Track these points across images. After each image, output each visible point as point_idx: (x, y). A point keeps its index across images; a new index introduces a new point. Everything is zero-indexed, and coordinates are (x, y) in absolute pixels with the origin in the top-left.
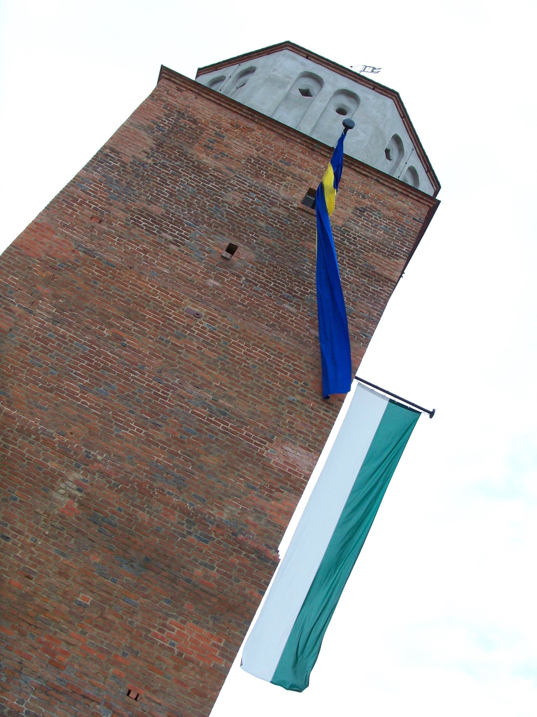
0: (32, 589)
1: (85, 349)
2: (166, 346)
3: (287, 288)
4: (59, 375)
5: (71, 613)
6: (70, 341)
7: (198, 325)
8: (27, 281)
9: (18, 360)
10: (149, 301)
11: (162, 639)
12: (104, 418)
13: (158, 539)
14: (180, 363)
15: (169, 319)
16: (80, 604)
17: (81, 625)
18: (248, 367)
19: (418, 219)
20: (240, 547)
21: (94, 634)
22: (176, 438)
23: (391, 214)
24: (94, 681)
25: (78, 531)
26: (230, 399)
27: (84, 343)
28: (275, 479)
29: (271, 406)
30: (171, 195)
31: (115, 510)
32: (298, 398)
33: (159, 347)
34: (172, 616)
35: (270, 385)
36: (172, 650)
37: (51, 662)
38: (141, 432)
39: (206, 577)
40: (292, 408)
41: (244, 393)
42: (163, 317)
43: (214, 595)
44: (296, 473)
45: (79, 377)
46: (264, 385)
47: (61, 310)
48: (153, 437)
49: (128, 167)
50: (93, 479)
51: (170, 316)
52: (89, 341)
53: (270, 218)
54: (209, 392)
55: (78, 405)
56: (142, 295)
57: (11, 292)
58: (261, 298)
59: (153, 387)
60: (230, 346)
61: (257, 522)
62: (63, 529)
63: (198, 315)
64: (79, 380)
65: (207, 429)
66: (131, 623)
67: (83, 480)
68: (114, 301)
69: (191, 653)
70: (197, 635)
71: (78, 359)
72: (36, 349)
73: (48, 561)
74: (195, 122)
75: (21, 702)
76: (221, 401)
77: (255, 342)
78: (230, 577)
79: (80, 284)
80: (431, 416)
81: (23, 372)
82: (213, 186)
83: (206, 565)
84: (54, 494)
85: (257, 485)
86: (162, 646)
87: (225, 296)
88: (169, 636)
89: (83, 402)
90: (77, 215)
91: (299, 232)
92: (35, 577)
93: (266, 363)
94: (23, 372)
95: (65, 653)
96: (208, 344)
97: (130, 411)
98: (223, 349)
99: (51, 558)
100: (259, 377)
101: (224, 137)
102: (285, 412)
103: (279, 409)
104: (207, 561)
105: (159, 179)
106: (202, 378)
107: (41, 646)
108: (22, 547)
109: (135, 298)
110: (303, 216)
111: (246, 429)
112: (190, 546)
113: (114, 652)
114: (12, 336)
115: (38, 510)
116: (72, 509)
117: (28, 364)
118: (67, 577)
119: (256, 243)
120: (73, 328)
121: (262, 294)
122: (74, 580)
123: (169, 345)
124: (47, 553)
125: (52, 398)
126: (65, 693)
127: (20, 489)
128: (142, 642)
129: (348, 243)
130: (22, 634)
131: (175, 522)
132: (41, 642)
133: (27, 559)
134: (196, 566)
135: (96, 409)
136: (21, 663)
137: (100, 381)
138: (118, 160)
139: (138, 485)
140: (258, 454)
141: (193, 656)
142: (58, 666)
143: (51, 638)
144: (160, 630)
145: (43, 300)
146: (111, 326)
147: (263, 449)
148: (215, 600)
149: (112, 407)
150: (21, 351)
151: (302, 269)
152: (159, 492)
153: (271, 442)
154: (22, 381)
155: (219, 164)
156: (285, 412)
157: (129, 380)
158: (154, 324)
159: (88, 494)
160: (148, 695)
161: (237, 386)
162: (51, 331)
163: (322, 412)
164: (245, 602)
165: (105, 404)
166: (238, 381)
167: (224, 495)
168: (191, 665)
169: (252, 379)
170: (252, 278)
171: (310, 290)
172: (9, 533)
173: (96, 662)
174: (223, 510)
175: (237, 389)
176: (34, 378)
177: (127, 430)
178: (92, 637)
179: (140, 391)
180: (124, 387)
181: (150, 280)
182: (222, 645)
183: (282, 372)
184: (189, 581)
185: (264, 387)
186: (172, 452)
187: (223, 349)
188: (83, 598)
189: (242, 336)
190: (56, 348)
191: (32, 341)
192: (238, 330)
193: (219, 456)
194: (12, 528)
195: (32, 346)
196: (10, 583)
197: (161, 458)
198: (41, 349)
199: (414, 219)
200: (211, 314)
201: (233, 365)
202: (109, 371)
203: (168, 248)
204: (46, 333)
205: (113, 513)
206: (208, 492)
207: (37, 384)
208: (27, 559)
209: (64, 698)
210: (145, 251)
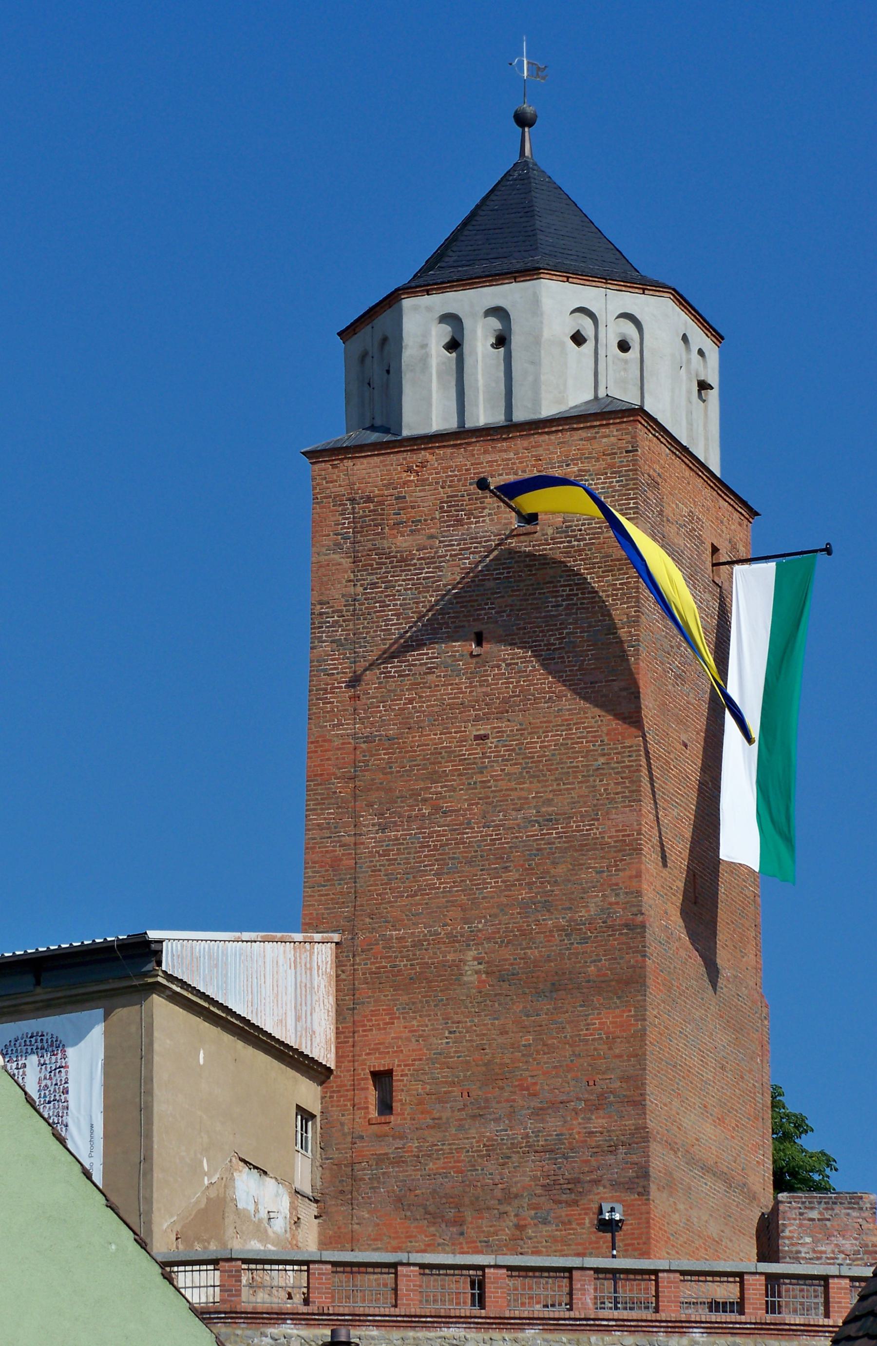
0: (490, 1055)
1: (419, 838)
2: (476, 788)
3: (545, 645)
4: (414, 877)
5: (523, 1055)
6: (404, 839)
7: (491, 748)
8: (340, 807)
9: (377, 885)
10: (441, 753)
11: (591, 1035)
12: (466, 890)
13: (552, 964)
14: (494, 797)
15: (465, 759)
16: (525, 1046)
17: (535, 1059)
18: (549, 760)
19: (630, 448)
20: (613, 931)
21: (546, 1060)
22: (527, 869)
23: (602, 464)
24: (562, 1090)
25: (496, 995)
26: (549, 802)
27: (416, 834)
28: (615, 852)
29: (584, 785)
30: (398, 615)
31: (512, 961)
32: (602, 760)
33: (472, 793)
34: (589, 1015)
35: (575, 764)
36: (601, 1038)
37: (530, 1095)
38: (498, 882)
39: (599, 970)
40: (602, 774)
41: (557, 788)
42: (460, 760)
43: (612, 980)
44: (629, 835)
45: (428, 868)
46: (569, 768)
47: (381, 815)
48: (509, 881)
49: (344, 613)
50: (484, 948)
51: (464, 755)
52: (417, 829)
53: (495, 570)
54: (529, 808)
55: (442, 892)
56: (433, 751)
57: (335, 827)
58: (528, 676)
59: (486, 836)
60: (526, 748)
61: (618, 900)
62: (485, 1001)
63: (484, 737)
64: (431, 870)
65: (545, 844)
66: (565, 1037)
67: (478, 954)
68: (415, 775)
69: (614, 1032)
70: (613, 1017)
71: (419, 852)
72: (383, 865)
73: (489, 1030)
74: (369, 500)
75: (525, 1128)
76: (544, 810)
77: (544, 729)
78: (616, 959)
79: (380, 779)
80: (829, 553)
81: (387, 893)
82: (426, 573)
83: (595, 961)
84: (465, 979)
85: (603, 867)
86: (593, 1040)
87: (498, 698)
88: (594, 1029)
89: (444, 888)
90: (337, 707)
91: (527, 566)
92: (487, 1047)
93: (562, 744)
94: (387, 893)
95: (535, 1084)
96: (507, 760)
97: (482, 870)
98: (521, 757)
99: (490, 1026)
100: (562, 763)
101: (405, 497)
102: (597, 782)
103: (592, 783)
104: (594, 958)
105: (378, 605)
106: (519, 799)
107: (517, 1089)
108: (467, 1032)
109: (428, 759)
110: (522, 542)
111: (574, 822)
112: (576, 955)
113: (565, 1063)
114: (361, 867)
115: (462, 998)
116: (484, 981)
117: (386, 884)
118: (507, 1033)
119: (496, 613)
120: (400, 826)
121: (526, 671)
122: (513, 1032)
123: (478, 785)
124: (484, 1025)
125: (420, 900)
126: (549, 1107)
127: (441, 991)
128: (579, 1045)
129: (576, 543)
130: (501, 1088)
131: (558, 942)
132: (516, 1086)
133: (475, 1038)
134: (589, 967)
135: (457, 886)
136: (511, 1106)
137: (445, 859)
138: (333, 612)
139: (518, 930)
140: (593, 839)
141: (618, 1033)
142: (535, 1095)
143: (520, 1080)
144: (587, 1030)
145: (363, 816)
146: (425, 800)
147: (595, 831)
148: (613, 983)
149: (467, 876)
150: (375, 876)
151: (548, 611)
152: (536, 925)
153: (598, 820)
154: (392, 902)
155: (421, 539)
156: (597, 782)
157: (465, 843)
158: (456, 773)
159: (487, 962)
160: (601, 1077)
161: (549, 786)
162: (385, 841)
163: (626, 759)
164: (634, 972)
165: (460, 877)
166: (547, 781)
167: (584, 893)
168: (619, 1040)
169: (557, 769)
170: (512, 659)
171: (565, 631)
172: (453, 1027)
173: (557, 1077)
174: (588, 906)
175: (551, 788)
176: (398, 892)
177: (487, 888)
178: (545, 1063)
179: (479, 846)
180: (466, 852)
181: (430, 730)
182: (633, 1013)
183: (577, 743)
184: (588, 981)
185: (570, 770)
186: (528, 884)
187: (521, 757)
188: (526, 1040)
189: (530, 731)
190: (398, 854)
191: (377, 861)
192: (524, 727)
193: (564, 862)
194: (453, 1023)
195: (380, 865)
196: (474, 1061)
197: (524, 894)
198: (387, 863)
199: (627, 452)
200: (495, 728)
201: (536, 767)
202: (447, 845)
203: (426, 683)
204: (382, 846)
205: (512, 964)
206: (571, 899)
207: (403, 896)
208: (475, 1038)
209: (550, 1111)
210: (411, 701)
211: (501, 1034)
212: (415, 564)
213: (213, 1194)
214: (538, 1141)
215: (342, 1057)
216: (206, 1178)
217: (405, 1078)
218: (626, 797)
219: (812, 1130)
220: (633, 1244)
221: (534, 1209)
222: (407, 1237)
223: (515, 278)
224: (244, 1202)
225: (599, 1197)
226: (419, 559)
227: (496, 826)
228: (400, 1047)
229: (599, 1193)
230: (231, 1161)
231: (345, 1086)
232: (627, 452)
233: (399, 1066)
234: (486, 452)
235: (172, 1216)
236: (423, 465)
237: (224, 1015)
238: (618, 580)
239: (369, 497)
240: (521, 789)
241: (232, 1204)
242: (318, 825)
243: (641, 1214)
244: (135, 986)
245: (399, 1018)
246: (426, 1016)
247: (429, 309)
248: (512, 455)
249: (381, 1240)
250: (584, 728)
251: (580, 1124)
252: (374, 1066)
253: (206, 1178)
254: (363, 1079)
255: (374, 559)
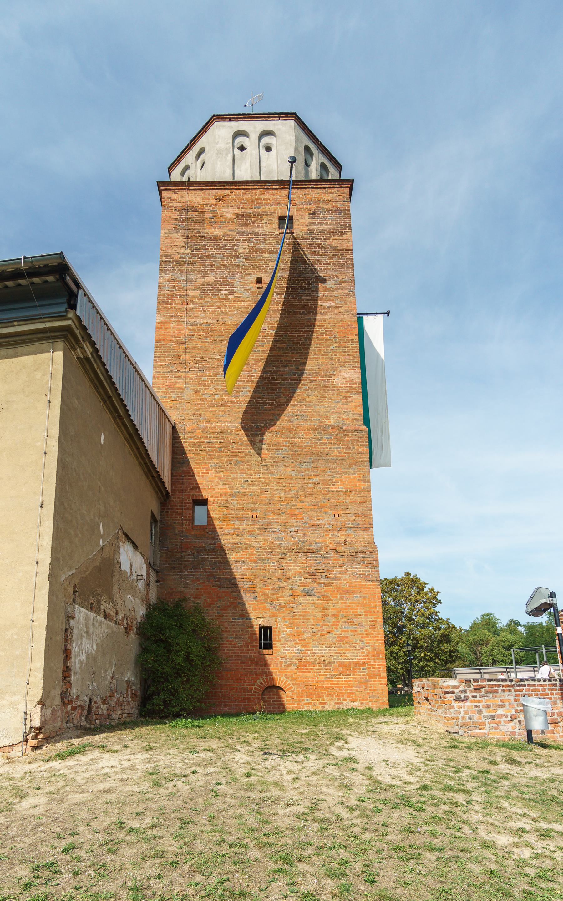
29: (325, 357)
32: (336, 345)
44: (353, 384)
54: (292, 366)
60: (289, 336)
108: (256, 481)
131: (313, 436)
168: (353, 492)
183: (321, 336)
199: (344, 201)
210: (219, 307)
211: (278, 483)
212: (222, 242)
213: (106, 555)
214: (305, 546)
215: (174, 490)
216: (101, 541)
217: (216, 505)
218: (351, 365)
220: (370, 612)
221: (303, 586)
222: (217, 598)
223: (279, 117)
224: (125, 567)
225: (346, 581)
226: (224, 240)
227: (271, 373)
228: (212, 486)
229: (346, 580)
230: (118, 533)
231: (177, 506)
232: (344, 201)
233: (212, 497)
234: (263, 194)
235: (71, 569)
238: (341, 259)
239: (196, 209)
240: (286, 356)
241: (117, 566)
242: (161, 365)
243: (375, 593)
245: (212, 470)
246: (229, 470)
249: (200, 598)
250: (325, 328)
251: (330, 538)
252: (196, 496)
253: (101, 541)
254: (188, 503)
255: (198, 238)
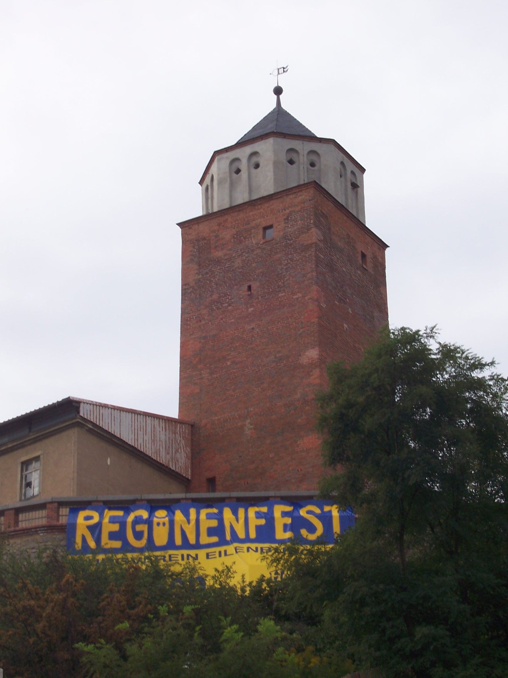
210: (222, 319)
219: (236, 572)
236: (226, 221)
237: (110, 437)
244: (112, 440)
247: (227, 158)
248: (262, 210)
